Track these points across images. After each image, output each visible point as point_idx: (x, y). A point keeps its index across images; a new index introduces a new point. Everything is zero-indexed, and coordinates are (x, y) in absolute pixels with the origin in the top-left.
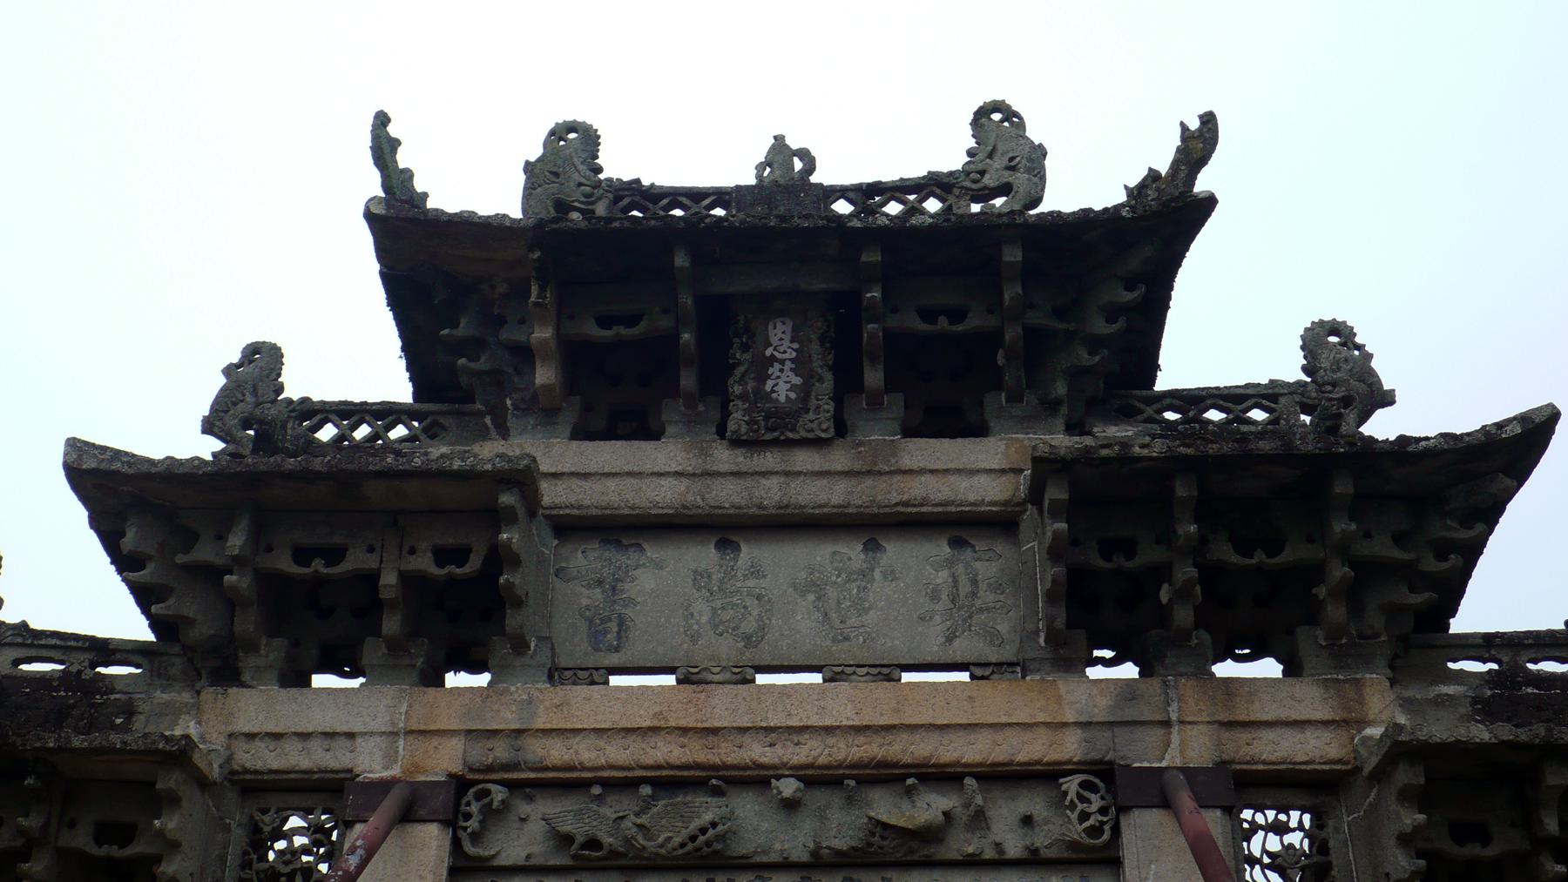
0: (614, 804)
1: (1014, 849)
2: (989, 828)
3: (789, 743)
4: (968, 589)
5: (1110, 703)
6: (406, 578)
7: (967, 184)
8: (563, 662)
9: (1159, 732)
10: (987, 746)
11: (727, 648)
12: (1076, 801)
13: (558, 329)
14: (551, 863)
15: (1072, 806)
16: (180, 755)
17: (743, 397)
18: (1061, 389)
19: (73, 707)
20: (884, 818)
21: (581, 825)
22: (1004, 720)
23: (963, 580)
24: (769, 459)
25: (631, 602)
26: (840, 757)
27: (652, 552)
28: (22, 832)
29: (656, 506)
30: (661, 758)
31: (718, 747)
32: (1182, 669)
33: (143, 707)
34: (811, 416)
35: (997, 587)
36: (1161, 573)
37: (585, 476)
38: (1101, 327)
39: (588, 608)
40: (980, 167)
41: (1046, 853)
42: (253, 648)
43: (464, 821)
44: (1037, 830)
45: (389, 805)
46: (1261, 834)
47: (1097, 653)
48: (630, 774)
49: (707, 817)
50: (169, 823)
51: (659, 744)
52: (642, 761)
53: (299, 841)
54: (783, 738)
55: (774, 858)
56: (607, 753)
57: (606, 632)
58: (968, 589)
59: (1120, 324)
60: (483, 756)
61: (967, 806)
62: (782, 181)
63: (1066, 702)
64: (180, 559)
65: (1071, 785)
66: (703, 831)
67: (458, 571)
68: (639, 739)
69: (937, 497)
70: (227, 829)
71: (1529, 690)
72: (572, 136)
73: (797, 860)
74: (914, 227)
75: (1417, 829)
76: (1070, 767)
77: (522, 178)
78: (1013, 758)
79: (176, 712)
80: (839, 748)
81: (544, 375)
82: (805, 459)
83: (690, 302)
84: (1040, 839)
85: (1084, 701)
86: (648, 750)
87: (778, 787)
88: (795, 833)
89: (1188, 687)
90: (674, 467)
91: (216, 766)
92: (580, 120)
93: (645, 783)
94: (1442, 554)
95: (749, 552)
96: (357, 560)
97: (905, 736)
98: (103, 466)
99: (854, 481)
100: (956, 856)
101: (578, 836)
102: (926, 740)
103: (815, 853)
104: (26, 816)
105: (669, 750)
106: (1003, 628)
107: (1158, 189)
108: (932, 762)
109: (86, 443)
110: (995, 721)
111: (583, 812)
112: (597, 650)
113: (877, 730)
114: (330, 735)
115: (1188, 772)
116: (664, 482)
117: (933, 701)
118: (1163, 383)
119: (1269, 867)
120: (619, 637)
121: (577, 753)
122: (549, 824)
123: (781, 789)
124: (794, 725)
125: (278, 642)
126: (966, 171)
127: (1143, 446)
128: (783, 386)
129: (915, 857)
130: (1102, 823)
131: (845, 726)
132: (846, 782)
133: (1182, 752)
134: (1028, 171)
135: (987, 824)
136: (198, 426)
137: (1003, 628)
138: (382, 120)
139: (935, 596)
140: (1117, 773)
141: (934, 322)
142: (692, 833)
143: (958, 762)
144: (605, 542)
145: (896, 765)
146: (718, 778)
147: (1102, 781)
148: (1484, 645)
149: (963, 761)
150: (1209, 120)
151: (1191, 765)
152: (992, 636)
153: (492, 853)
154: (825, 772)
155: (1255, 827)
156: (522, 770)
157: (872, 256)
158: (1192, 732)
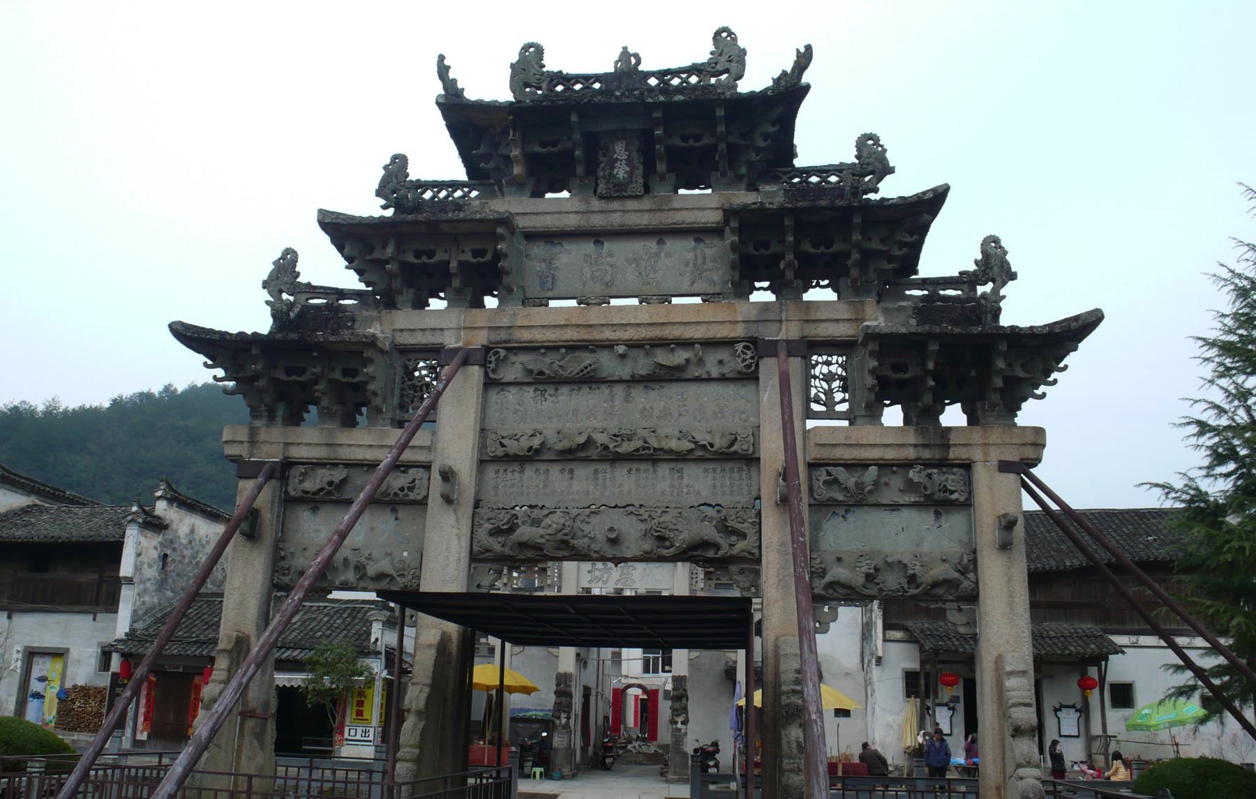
1: (715, 374)
4: (702, 260)
6: (460, 263)
7: (709, 69)
8: (529, 295)
9: (777, 325)
11: (598, 288)
13: (523, 149)
15: (739, 356)
16: (372, 342)
17: (604, 177)
18: (744, 170)
19: (331, 318)
20: (661, 362)
22: (712, 320)
23: (699, 256)
24: (616, 205)
25: (558, 269)
26: (643, 336)
27: (567, 246)
28: (313, 374)
29: (567, 226)
32: (789, 297)
33: (359, 318)
34: (633, 185)
35: (714, 260)
36: (781, 256)
37: (537, 214)
38: (761, 143)
39: (539, 271)
40: (715, 61)
41: (728, 376)
42: (401, 293)
45: (457, 359)
46: (820, 365)
47: (757, 285)
50: (370, 370)
53: (424, 372)
55: (616, 378)
57: (547, 282)
58: (702, 260)
59: (769, 141)
61: (696, 356)
62: (625, 70)
64: (368, 257)
65: (739, 347)
66: (586, 368)
67: (482, 260)
69: (689, 220)
70: (395, 368)
71: (939, 303)
72: (532, 50)
74: (675, 101)
75: (874, 368)
77: (510, 70)
79: (369, 321)
81: (517, 170)
82: (631, 205)
83: (578, 137)
84: (725, 370)
89: (790, 304)
90: (575, 209)
91: (387, 345)
92: (535, 42)
94: (902, 245)
95: (608, 246)
96: (440, 256)
98: (334, 221)
99: (652, 214)
100: (690, 377)
103: (632, 376)
104: (315, 368)
106: (716, 278)
107: (786, 80)
109: (326, 211)
112: (543, 290)
114: (434, 330)
115: (788, 342)
116: (571, 216)
118: (798, 163)
119: (822, 379)
120: (552, 285)
125: (410, 290)
126: (709, 63)
127: (770, 204)
128: (621, 171)
134: (737, 62)
136: (374, 193)
137: (716, 278)
138: (441, 58)
139: (687, 264)
141: (687, 142)
144: (547, 242)
145: (666, 339)
146: (593, 345)
148: (924, 283)
150: (809, 48)
152: (711, 282)
155: (817, 363)
157: (657, 115)
158: (792, 324)
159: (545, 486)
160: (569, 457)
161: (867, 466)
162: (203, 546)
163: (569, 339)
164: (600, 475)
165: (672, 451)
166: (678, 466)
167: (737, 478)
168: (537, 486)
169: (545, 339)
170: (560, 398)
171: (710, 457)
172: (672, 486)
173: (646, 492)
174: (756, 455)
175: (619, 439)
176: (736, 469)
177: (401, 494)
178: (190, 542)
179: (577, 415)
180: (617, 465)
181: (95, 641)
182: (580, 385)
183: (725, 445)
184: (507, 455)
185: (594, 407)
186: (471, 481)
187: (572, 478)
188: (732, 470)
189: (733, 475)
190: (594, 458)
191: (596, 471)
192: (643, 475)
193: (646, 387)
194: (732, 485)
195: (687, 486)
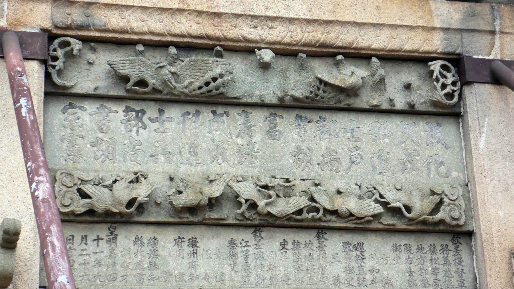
0: (150, 57)
1: (400, 104)
2: (385, 90)
3: (266, 27)
5: (461, 17)
9: (488, 38)
10: (387, 39)
12: (439, 76)
14: (112, 93)
15: (437, 80)
21: (134, 70)
22: (399, 23)
26: (298, 38)
30: (184, 30)
31: (221, 26)
41: (419, 107)
43: (52, 61)
44: (413, 93)
48: (163, 39)
49: (217, 71)
51: (183, 21)
52: (172, 31)
54: (262, 23)
55: (255, 100)
56: (149, 23)
60: (64, 18)
63: (435, 14)
66: (215, 79)
68: (170, 16)
73: (269, 102)
76: (434, 55)
78: (402, 47)
80: (297, 33)
85: (445, 15)
86: (176, 24)
87: (260, 55)
88: (268, 85)
93: (172, 45)
97: (337, 28)
100: (365, 106)
101: (133, 77)
102: (350, 32)
105: (190, 25)
108: (353, 47)
110: (393, 23)
111: (136, 61)
113: (321, 23)
117: (355, 7)
121: (128, 22)
122: (113, 68)
123: (263, 56)
124: (271, 15)
129: (341, 105)
130: (454, 91)
131: (302, 19)
132: (300, 55)
133: (502, 50)
135: (385, 87)
140: (465, 61)
142: (207, 81)
143: (370, 47)
145: (331, 46)
146: (220, 46)
147: (452, 65)
149: (372, 47)
151: (506, 59)
153: (72, 84)
154: (287, 48)
156: (91, 30)
159: (153, 265)
160: (191, 219)
163: (184, 31)
164: (239, 250)
165: (351, 215)
166: (355, 239)
167: (441, 260)
168: (139, 264)
169: (146, 29)
170: (167, 125)
171: (404, 227)
172: (349, 270)
173: (311, 278)
174: (469, 228)
175: (272, 192)
176: (438, 248)
179: (196, 154)
180: (263, 234)
182: (198, 108)
183: (428, 210)
184: (91, 212)
185: (223, 142)
186: (51, 264)
187: (195, 253)
188: (433, 249)
189: (434, 256)
190: (231, 221)
191: (232, 243)
192: (304, 252)
193: (299, 117)
194: (435, 272)
195: (372, 271)
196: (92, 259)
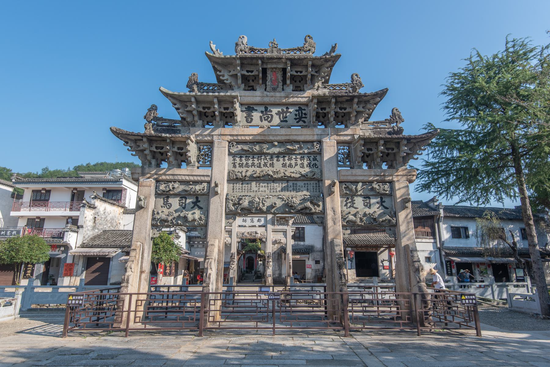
150: (336, 44)
161: (358, 182)
162: (109, 214)
177: (200, 192)
178: (104, 213)
181: (518, 228)
196: (238, 188)
